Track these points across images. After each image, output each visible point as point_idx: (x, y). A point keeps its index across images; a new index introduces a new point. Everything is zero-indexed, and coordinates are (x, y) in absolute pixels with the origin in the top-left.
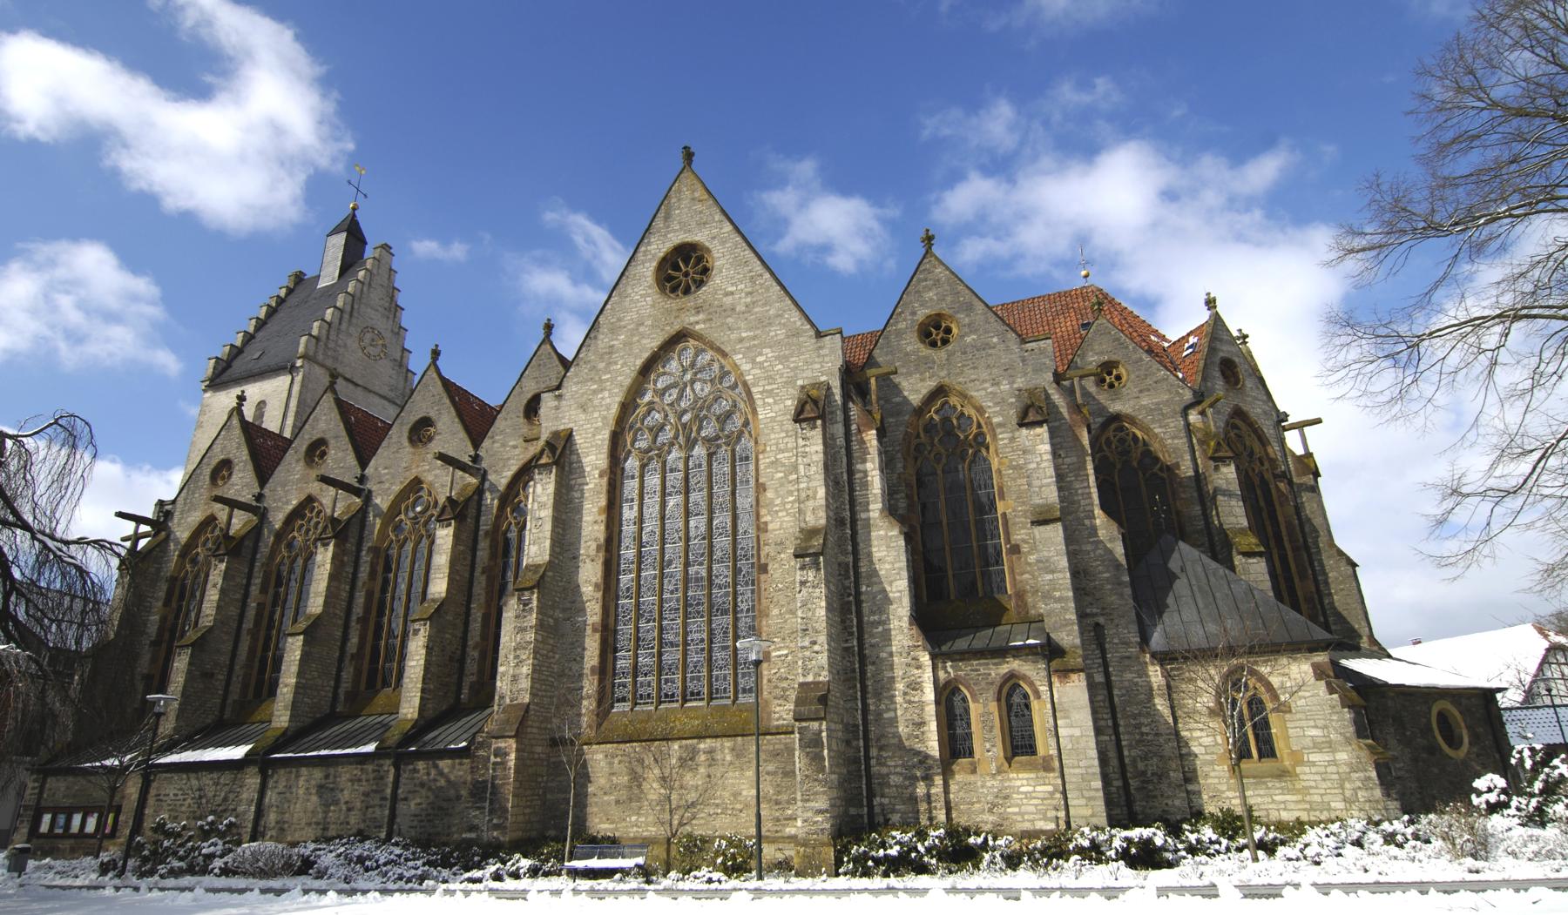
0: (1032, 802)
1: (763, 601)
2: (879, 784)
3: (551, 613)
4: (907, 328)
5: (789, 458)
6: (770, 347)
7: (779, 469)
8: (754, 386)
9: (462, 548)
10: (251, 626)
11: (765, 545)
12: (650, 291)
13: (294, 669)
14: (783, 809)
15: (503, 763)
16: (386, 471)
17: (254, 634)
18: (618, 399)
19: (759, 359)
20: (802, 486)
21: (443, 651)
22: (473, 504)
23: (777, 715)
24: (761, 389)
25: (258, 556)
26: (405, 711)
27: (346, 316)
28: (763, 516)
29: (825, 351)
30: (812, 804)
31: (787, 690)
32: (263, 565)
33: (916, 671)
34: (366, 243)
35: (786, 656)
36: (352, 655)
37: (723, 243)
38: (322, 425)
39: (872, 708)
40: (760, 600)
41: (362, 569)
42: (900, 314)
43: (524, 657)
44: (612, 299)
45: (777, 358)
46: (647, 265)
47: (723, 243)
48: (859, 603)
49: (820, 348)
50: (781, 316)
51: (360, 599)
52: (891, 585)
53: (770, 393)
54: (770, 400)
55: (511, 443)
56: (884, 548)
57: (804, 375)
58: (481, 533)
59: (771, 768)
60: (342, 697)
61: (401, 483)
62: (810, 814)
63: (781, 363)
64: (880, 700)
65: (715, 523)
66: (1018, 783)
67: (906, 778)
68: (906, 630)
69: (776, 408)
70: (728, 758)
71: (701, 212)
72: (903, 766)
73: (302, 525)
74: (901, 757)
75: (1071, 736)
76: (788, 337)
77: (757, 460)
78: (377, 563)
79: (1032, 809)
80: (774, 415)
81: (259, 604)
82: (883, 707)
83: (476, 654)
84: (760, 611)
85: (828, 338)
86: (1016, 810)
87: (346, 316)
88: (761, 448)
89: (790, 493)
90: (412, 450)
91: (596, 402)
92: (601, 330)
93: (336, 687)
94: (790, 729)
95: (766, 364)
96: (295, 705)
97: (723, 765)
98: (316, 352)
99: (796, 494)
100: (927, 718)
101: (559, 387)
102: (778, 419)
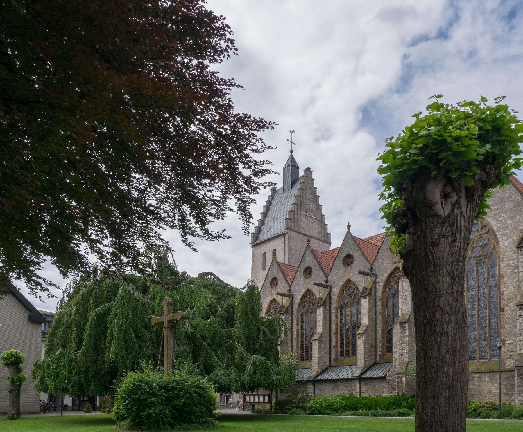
1: (502, 322)
5: (514, 263)
6: (505, 213)
7: (510, 268)
8: (498, 231)
9: (371, 306)
10: (296, 337)
11: (503, 300)
13: (317, 351)
14: (510, 397)
15: (401, 381)
16: (336, 278)
17: (297, 339)
19: (500, 219)
22: (373, 289)
23: (508, 365)
24: (501, 233)
25: (293, 312)
26: (359, 365)
27: (299, 206)
28: (502, 288)
31: (512, 355)
32: (296, 315)
34: (298, 168)
35: (512, 343)
36: (334, 346)
38: (308, 261)
40: (500, 322)
41: (333, 315)
43: (405, 346)
45: (509, 218)
50: (511, 197)
51: (334, 326)
53: (506, 234)
54: (506, 238)
55: (386, 262)
58: (377, 299)
59: (505, 383)
60: (332, 360)
61: (343, 282)
63: (511, 220)
65: (480, 292)
69: (509, 241)
70: (487, 379)
73: (307, 300)
76: (514, 207)
77: (499, 265)
80: (507, 244)
81: (297, 329)
83: (381, 344)
84: (500, 326)
87: (299, 206)
88: (501, 259)
89: (515, 278)
90: (345, 268)
93: (330, 357)
94: (513, 370)
95: (503, 221)
96: (319, 363)
98: (291, 226)
99: (517, 278)
102: (509, 246)
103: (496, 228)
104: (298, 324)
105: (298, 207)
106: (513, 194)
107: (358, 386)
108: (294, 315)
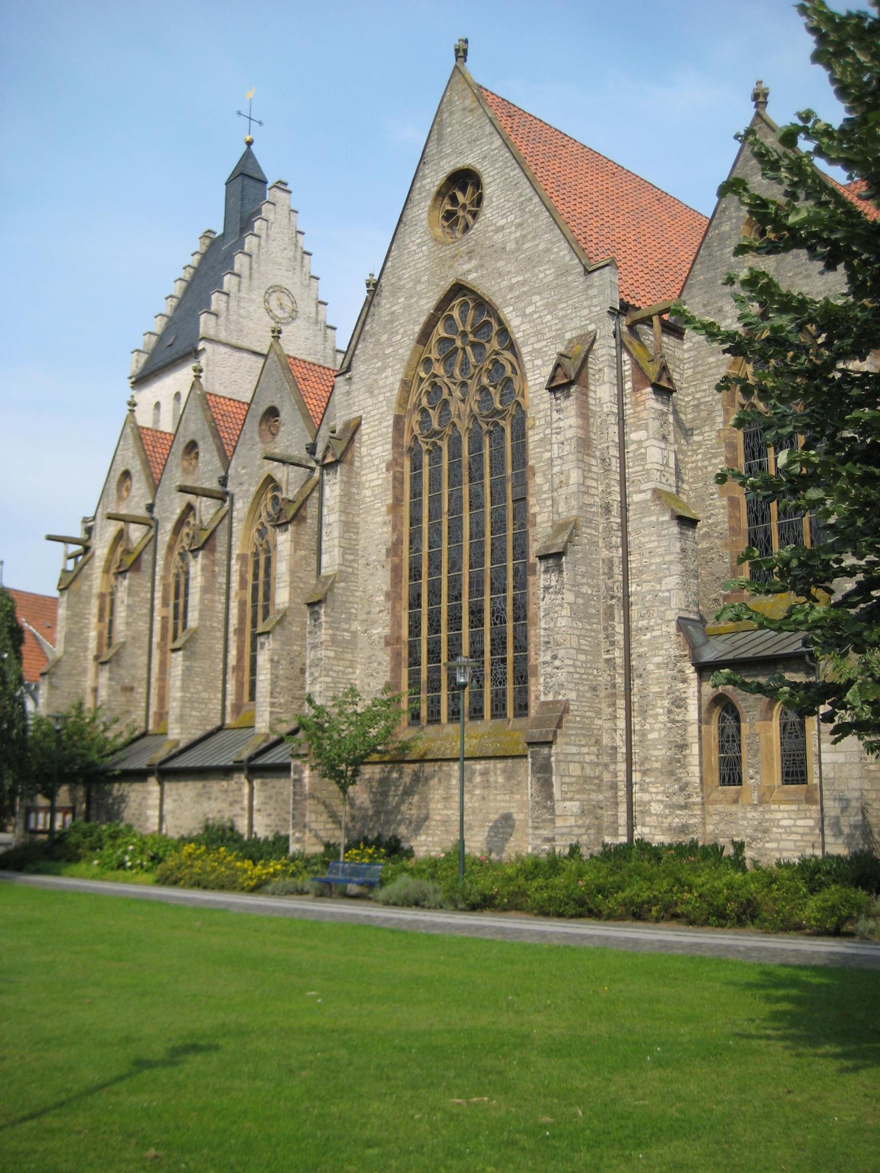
0: (791, 838)
2: (641, 812)
3: (347, 626)
4: (732, 229)
6: (540, 293)
12: (426, 238)
18: (399, 377)
19: (529, 310)
20: (556, 469)
21: (291, 663)
29: (593, 292)
30: (541, 832)
33: (681, 685)
37: (493, 162)
39: (637, 727)
42: (724, 211)
44: (392, 254)
46: (423, 204)
47: (493, 162)
48: (627, 606)
49: (590, 287)
52: (660, 583)
56: (654, 538)
57: (573, 325)
62: (539, 842)
63: (550, 313)
64: (645, 719)
66: (779, 815)
67: (666, 806)
68: (673, 637)
70: (501, 780)
71: (471, 126)
72: (664, 793)
74: (662, 783)
75: (835, 763)
78: (246, 572)
79: (791, 845)
82: (647, 727)
85: (596, 274)
86: (773, 845)
91: (381, 383)
92: (383, 294)
97: (496, 787)
100: (690, 740)
101: (349, 369)
103: (521, 334)
104: (165, 603)
105: (240, 282)
106: (554, 243)
107: (246, 790)
108: (157, 578)
